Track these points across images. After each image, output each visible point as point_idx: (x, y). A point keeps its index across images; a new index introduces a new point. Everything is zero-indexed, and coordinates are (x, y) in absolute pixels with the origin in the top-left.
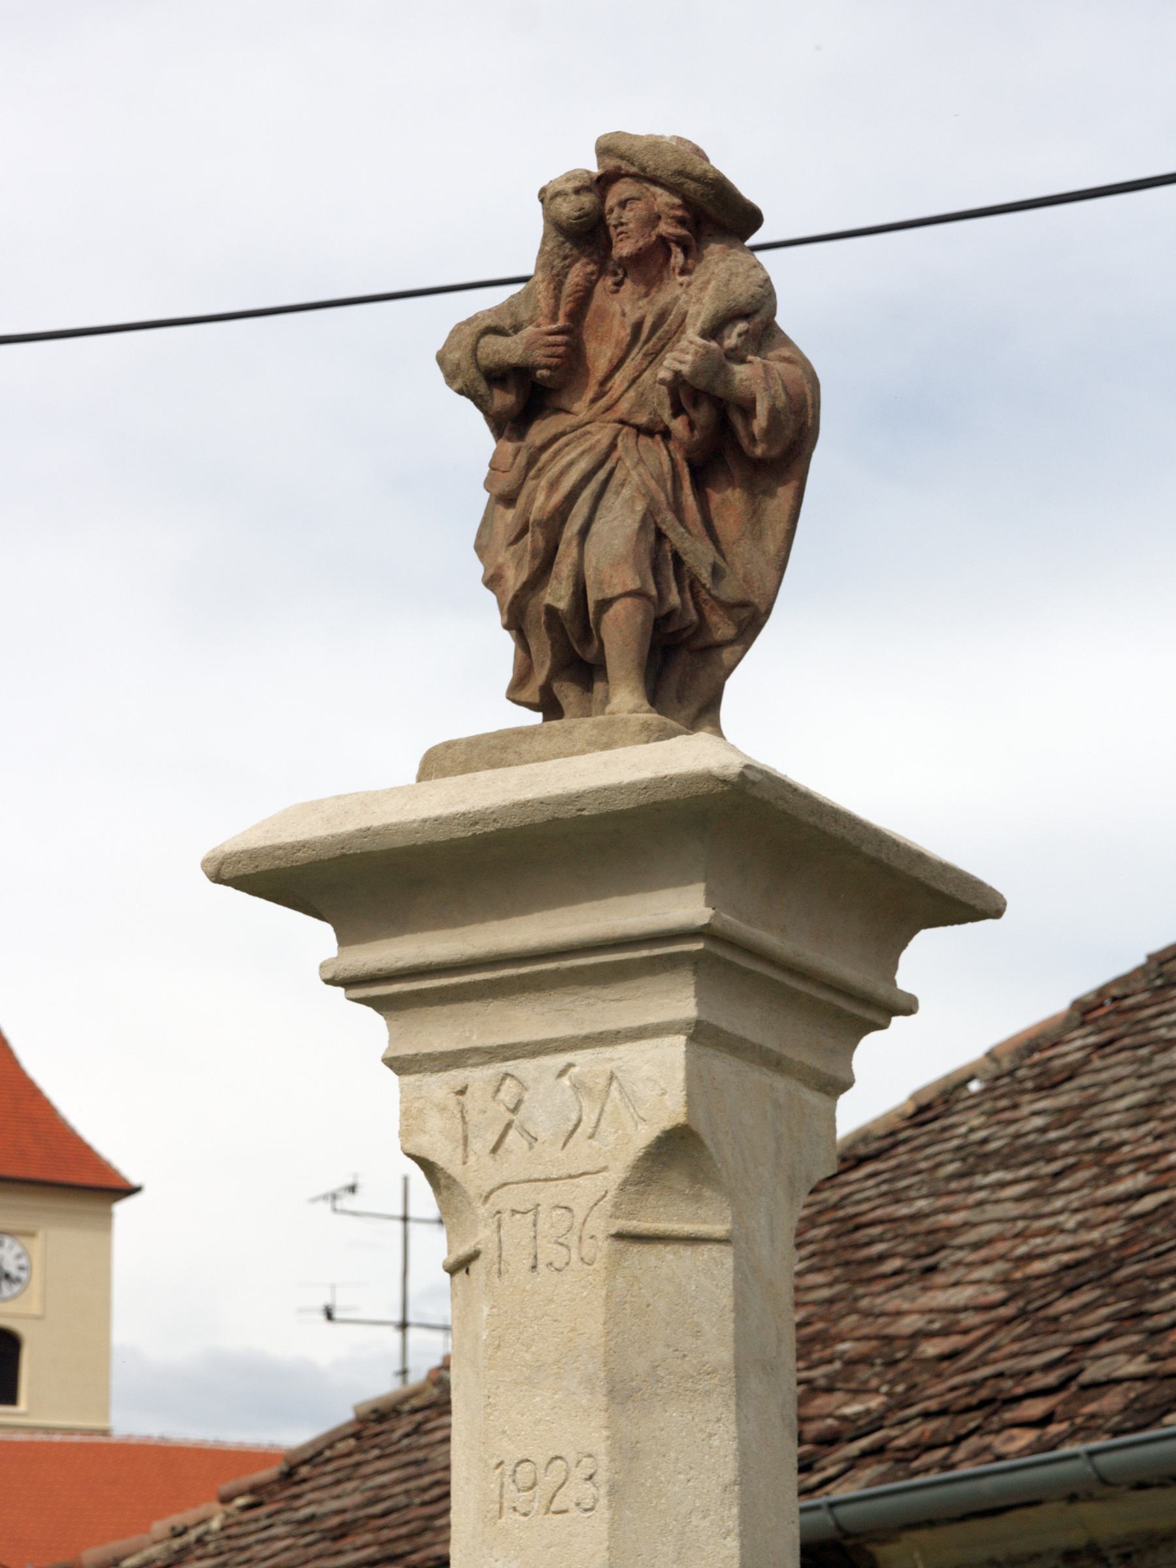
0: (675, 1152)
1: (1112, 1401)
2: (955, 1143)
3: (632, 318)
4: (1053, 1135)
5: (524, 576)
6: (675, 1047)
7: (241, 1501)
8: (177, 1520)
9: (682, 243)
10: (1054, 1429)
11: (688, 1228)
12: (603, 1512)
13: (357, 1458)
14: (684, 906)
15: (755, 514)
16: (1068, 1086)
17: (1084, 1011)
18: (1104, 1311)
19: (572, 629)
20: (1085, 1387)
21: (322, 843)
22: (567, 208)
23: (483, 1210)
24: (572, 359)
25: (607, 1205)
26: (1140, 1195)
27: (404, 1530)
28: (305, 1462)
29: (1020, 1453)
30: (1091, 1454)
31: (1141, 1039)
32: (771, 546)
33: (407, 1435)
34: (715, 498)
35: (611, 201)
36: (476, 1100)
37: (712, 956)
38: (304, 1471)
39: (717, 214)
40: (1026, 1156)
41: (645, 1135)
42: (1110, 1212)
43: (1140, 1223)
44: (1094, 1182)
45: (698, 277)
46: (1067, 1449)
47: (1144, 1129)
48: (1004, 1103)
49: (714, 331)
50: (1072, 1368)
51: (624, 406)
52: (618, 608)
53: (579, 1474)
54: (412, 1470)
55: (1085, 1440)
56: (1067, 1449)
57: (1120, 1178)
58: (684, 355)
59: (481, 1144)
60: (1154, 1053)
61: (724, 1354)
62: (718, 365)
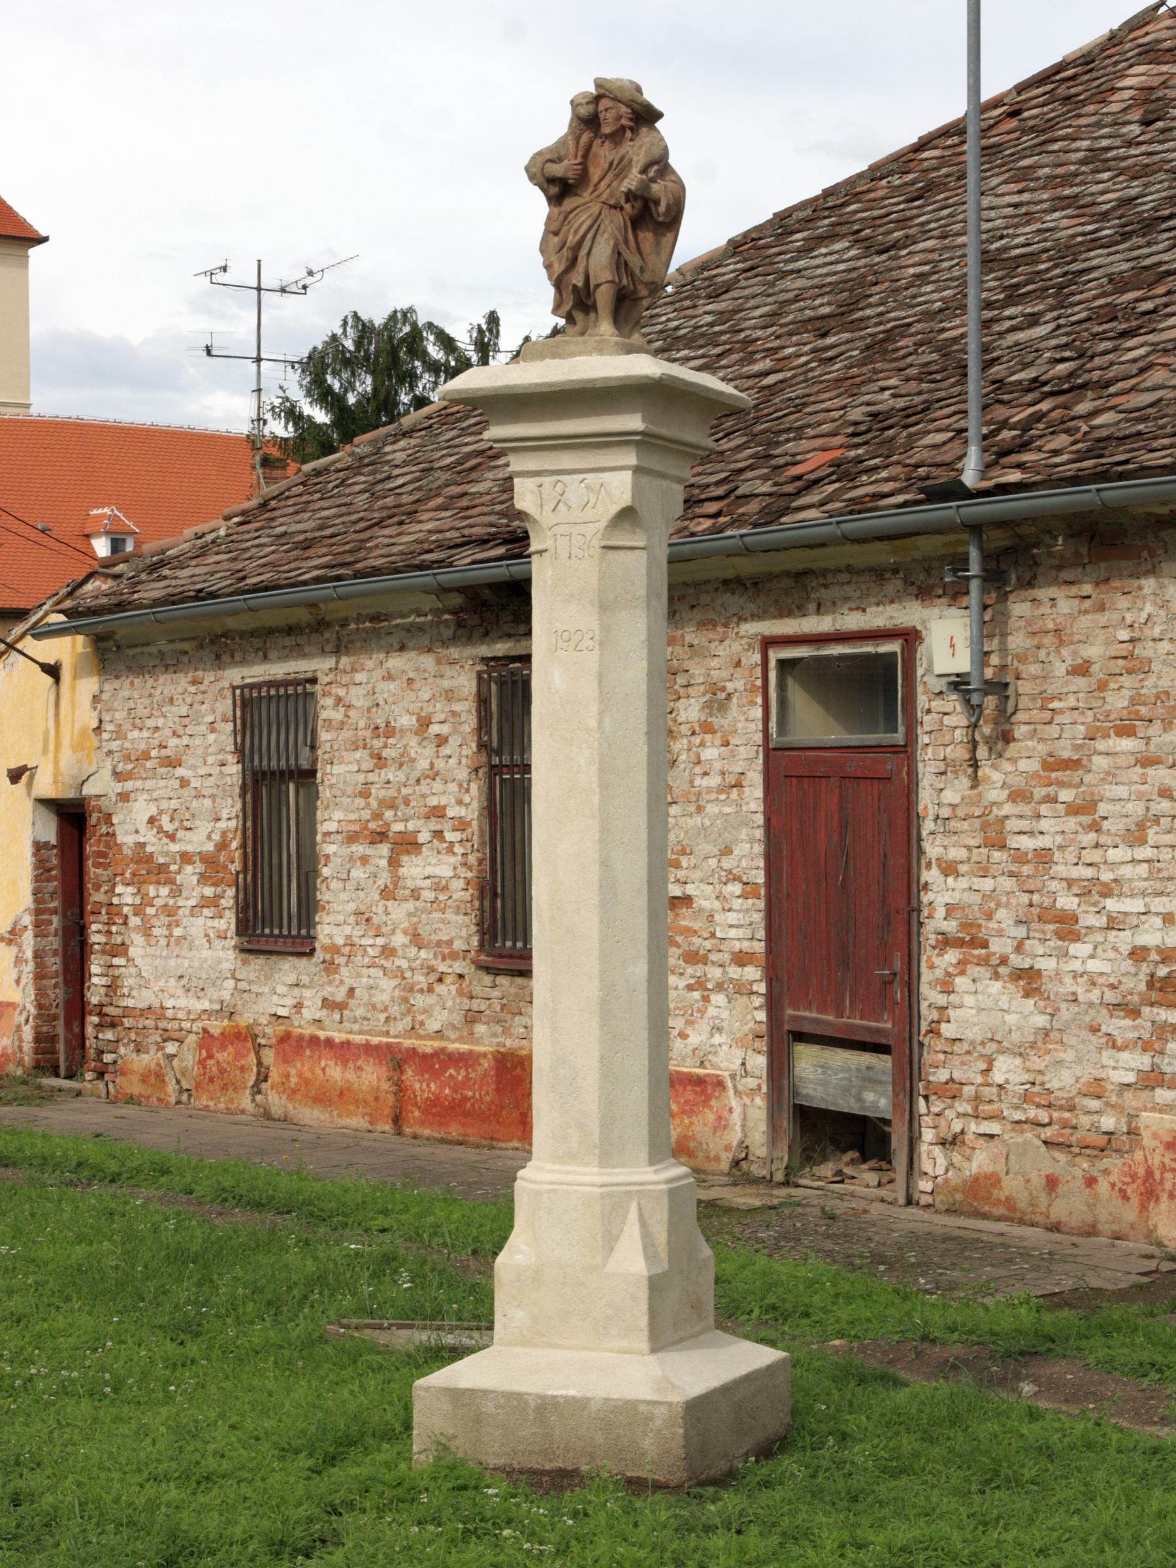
0: (627, 516)
1: (753, 507)
2: (659, 327)
3: (610, 158)
4: (717, 329)
5: (563, 268)
6: (628, 475)
7: (236, 520)
8: (200, 528)
9: (632, 129)
10: (722, 520)
11: (630, 544)
12: (597, 652)
13: (305, 498)
14: (633, 422)
15: (658, 244)
16: (725, 296)
17: (736, 246)
18: (749, 452)
19: (583, 294)
20: (738, 497)
21: (488, 389)
22: (584, 111)
23: (549, 534)
24: (583, 176)
25: (599, 535)
26: (767, 374)
27: (347, 547)
28: (273, 498)
29: (704, 532)
30: (742, 536)
31: (769, 269)
32: (664, 258)
33: (337, 487)
34: (641, 235)
35: (601, 108)
36: (546, 490)
37: (644, 442)
38: (273, 503)
39: (646, 116)
40: (701, 342)
41: (615, 509)
42: (750, 383)
43: (766, 392)
44: (742, 362)
45: (637, 142)
46: (729, 533)
47: (770, 331)
48: (688, 303)
49: (644, 171)
50: (732, 485)
51: (604, 196)
52: (603, 287)
53: (588, 637)
54: (344, 509)
55: (738, 528)
56: (729, 533)
57: (756, 361)
58: (632, 180)
59: (548, 507)
60: (776, 280)
61: (643, 592)
62: (645, 185)
